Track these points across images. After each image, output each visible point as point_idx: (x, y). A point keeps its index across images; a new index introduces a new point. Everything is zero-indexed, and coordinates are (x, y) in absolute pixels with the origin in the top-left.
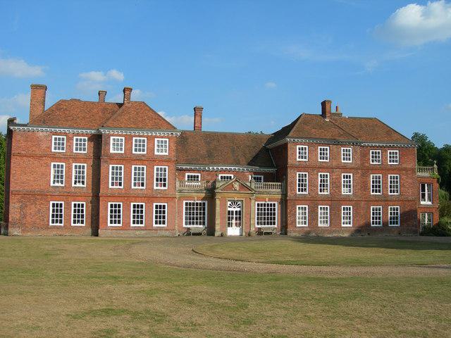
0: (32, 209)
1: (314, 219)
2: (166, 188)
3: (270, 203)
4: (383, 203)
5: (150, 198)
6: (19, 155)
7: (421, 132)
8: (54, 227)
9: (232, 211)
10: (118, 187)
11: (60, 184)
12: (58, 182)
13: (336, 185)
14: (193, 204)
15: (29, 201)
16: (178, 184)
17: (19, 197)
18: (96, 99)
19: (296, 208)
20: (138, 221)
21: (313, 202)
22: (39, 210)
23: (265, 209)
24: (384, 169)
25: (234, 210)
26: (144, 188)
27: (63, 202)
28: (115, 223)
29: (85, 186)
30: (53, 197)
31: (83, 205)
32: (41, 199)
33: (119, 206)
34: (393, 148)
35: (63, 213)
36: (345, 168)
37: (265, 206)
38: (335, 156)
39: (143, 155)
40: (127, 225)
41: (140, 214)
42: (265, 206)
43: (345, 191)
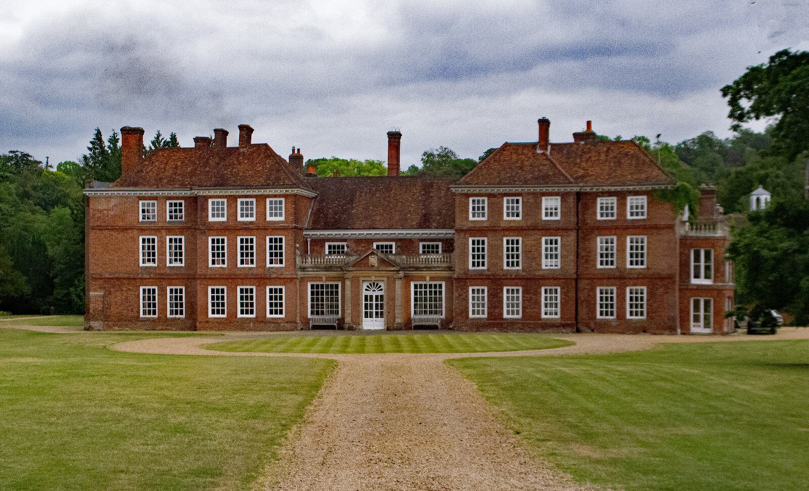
0: (117, 297)
1: (495, 307)
2: (283, 265)
3: (433, 283)
4: (617, 282)
5: (262, 279)
6: (100, 228)
7: (435, 148)
8: (148, 319)
9: (371, 297)
10: (221, 265)
11: (151, 264)
12: (149, 260)
13: (533, 255)
14: (322, 286)
15: (114, 287)
16: (298, 259)
17: (101, 282)
18: (382, 156)
19: (468, 291)
20: (247, 311)
21: (496, 282)
22: (127, 298)
23: (426, 292)
24: (621, 228)
25: (374, 294)
26: (254, 266)
27: (156, 288)
28: (247, 313)
29: (183, 265)
30: (143, 281)
31: (181, 290)
32: (129, 284)
33: (223, 291)
34: (636, 193)
35: (157, 301)
36: (549, 229)
37: (426, 287)
38: (496, 210)
39: (251, 223)
40: (233, 314)
41: (279, 308)
42: (426, 287)
43: (547, 264)
